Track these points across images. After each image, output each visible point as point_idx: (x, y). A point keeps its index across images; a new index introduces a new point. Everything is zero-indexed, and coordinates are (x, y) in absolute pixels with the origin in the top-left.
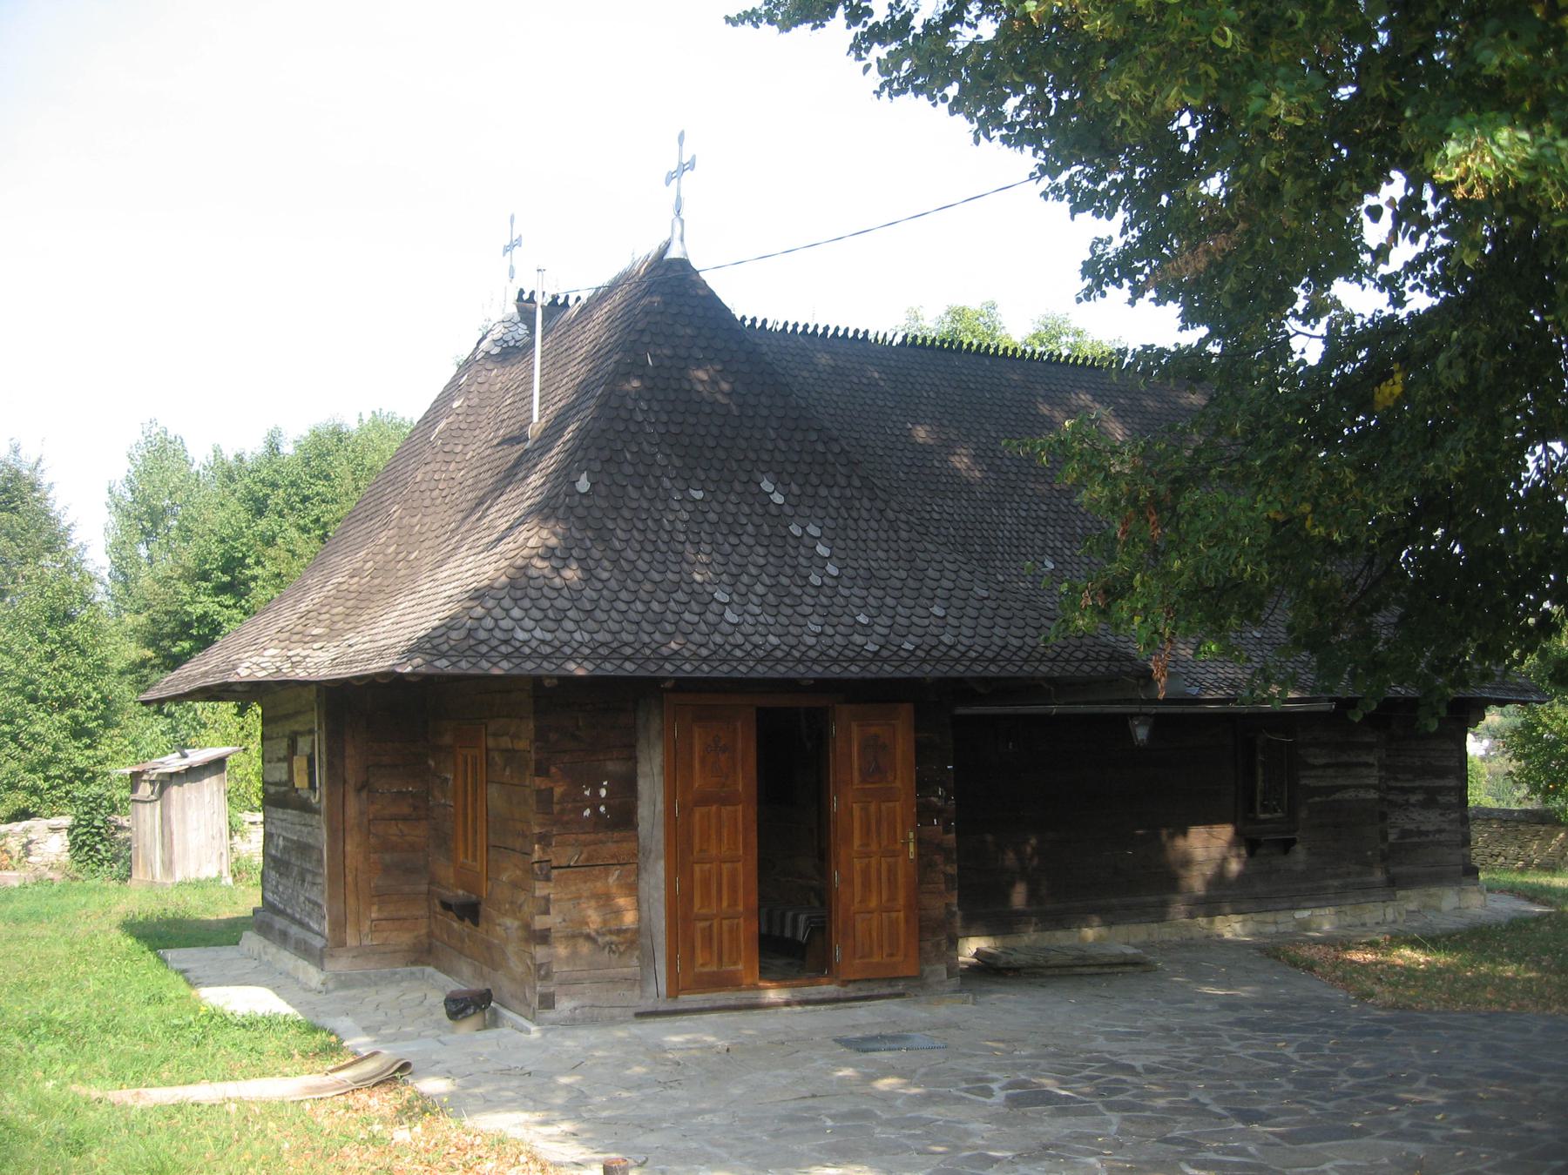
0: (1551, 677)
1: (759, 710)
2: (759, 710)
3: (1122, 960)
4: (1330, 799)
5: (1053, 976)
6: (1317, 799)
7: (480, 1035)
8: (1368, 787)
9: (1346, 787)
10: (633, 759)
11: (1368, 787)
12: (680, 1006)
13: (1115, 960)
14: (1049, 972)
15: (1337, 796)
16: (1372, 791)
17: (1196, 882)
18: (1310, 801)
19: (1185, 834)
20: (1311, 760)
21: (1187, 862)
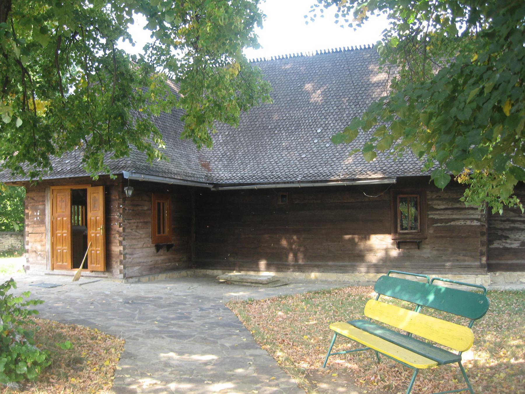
0: (25, 156)
1: (71, 189)
2: (71, 189)
3: (255, 281)
4: (447, 225)
5: (237, 285)
6: (439, 225)
7: (394, 306)
8: (472, 220)
9: (458, 219)
10: (45, 205)
11: (472, 220)
12: (54, 273)
13: (253, 281)
14: (235, 283)
15: (452, 223)
16: (475, 221)
17: (373, 258)
18: (435, 225)
19: (369, 239)
20: (436, 207)
21: (370, 250)
